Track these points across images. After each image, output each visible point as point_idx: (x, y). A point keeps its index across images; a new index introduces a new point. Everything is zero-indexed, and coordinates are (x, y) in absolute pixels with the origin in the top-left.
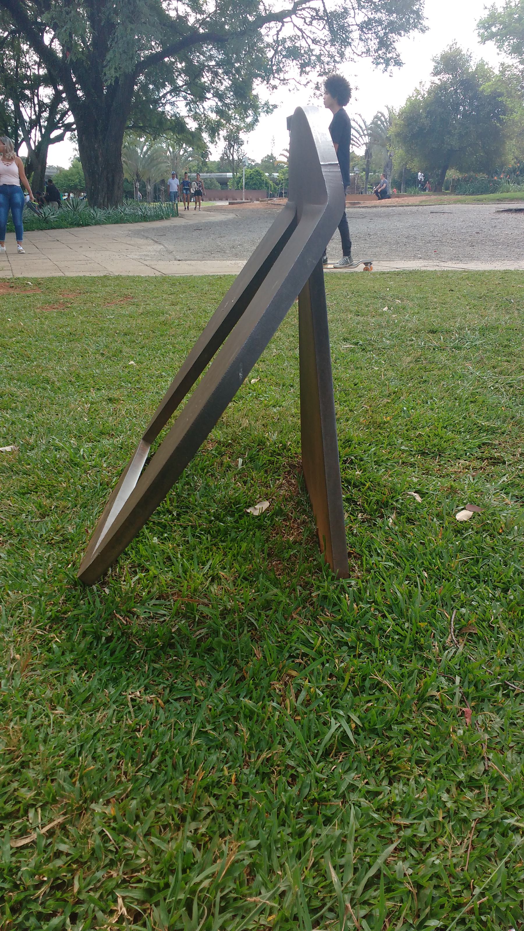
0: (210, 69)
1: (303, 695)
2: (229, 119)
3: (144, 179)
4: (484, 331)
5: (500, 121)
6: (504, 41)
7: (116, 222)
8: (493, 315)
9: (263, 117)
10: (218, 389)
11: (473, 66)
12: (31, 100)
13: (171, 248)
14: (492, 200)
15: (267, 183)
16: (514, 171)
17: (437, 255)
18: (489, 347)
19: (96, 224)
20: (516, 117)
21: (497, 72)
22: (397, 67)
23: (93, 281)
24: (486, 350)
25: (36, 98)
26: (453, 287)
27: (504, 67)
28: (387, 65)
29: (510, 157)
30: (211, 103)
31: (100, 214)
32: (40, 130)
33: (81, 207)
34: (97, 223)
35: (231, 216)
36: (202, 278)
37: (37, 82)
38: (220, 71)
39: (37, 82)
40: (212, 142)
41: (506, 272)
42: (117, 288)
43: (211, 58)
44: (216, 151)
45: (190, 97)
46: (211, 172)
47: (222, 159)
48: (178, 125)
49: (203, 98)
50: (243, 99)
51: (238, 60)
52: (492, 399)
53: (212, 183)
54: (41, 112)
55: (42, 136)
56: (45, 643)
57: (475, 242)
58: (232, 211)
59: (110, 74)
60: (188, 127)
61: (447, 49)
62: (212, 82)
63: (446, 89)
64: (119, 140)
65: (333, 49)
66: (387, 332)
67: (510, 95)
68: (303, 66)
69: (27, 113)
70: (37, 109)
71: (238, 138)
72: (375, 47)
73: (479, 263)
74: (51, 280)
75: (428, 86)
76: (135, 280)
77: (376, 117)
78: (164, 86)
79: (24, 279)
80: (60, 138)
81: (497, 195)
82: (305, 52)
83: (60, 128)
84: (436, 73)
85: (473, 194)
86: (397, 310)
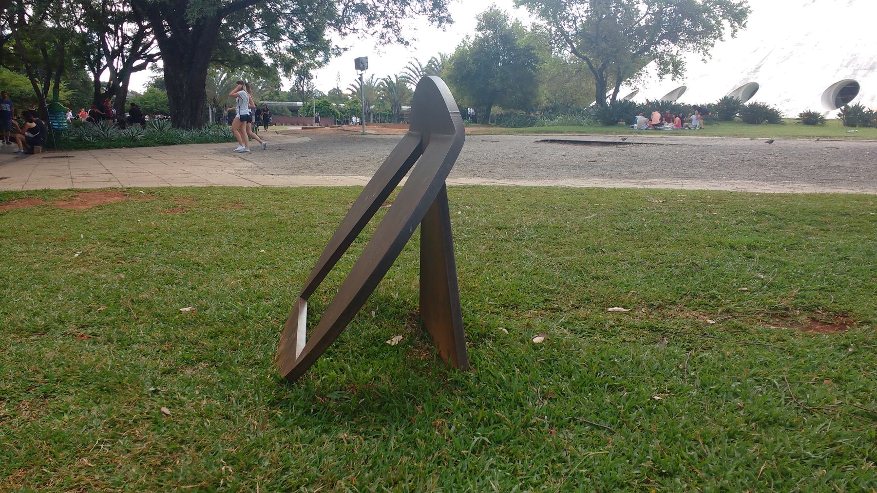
0: (285, 15)
1: (453, 428)
2: (301, 57)
3: (221, 105)
4: (537, 228)
5: (534, 68)
6: (534, 7)
7: (201, 142)
8: (542, 218)
9: (333, 59)
10: (396, 240)
11: (510, 23)
12: (115, 33)
13: (261, 164)
14: (531, 132)
15: (334, 112)
16: (547, 109)
17: (491, 173)
18: (542, 239)
19: (181, 143)
20: (546, 66)
21: (529, 30)
22: (448, 25)
23: (202, 190)
24: (541, 242)
25: (119, 32)
26: (509, 198)
27: (535, 27)
28: (441, 22)
29: (543, 98)
30: (285, 44)
31: (185, 134)
32: (123, 61)
33: (166, 129)
34: (183, 142)
35: (307, 139)
36: (297, 188)
37: (120, 18)
38: (295, 18)
39: (120, 18)
40: (286, 76)
41: (548, 188)
42: (226, 196)
43: (286, 7)
44: (287, 84)
45: (266, 38)
46: (282, 101)
47: (293, 90)
48: (256, 61)
49: (279, 40)
50: (315, 41)
51: (310, 11)
52: (549, 271)
53: (283, 111)
54: (124, 43)
55: (124, 64)
56: (272, 416)
57: (521, 165)
58: (307, 135)
59: (192, 15)
60: (265, 62)
61: (488, 10)
62: (287, 27)
63: (488, 43)
64: (203, 72)
65: (395, 7)
66: (465, 229)
67: (540, 48)
68: (369, 19)
69: (111, 43)
70: (120, 40)
71: (307, 73)
72: (430, 7)
73: (526, 181)
74: (161, 189)
75: (472, 39)
76: (238, 189)
77: (431, 61)
78: (242, 27)
79: (136, 188)
80: (142, 67)
81: (535, 128)
82: (372, 9)
83: (142, 58)
84: (479, 29)
85: (514, 126)
86: (468, 213)
